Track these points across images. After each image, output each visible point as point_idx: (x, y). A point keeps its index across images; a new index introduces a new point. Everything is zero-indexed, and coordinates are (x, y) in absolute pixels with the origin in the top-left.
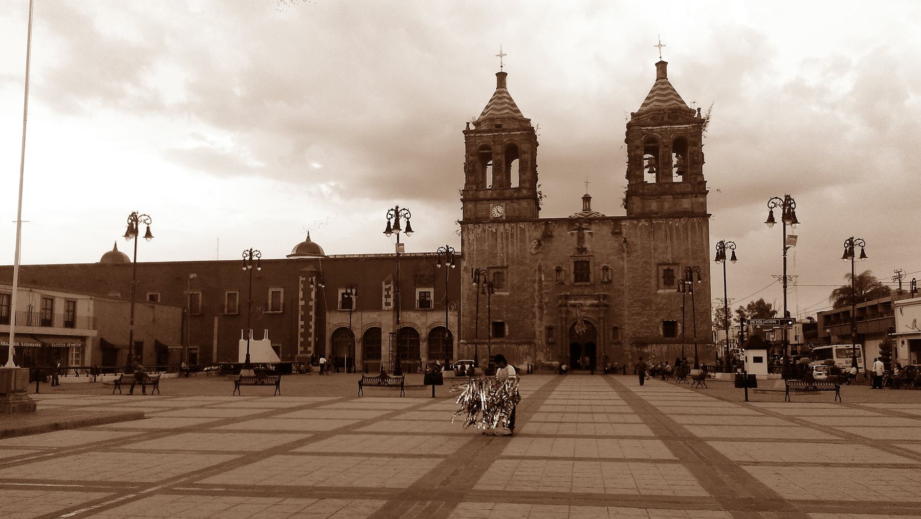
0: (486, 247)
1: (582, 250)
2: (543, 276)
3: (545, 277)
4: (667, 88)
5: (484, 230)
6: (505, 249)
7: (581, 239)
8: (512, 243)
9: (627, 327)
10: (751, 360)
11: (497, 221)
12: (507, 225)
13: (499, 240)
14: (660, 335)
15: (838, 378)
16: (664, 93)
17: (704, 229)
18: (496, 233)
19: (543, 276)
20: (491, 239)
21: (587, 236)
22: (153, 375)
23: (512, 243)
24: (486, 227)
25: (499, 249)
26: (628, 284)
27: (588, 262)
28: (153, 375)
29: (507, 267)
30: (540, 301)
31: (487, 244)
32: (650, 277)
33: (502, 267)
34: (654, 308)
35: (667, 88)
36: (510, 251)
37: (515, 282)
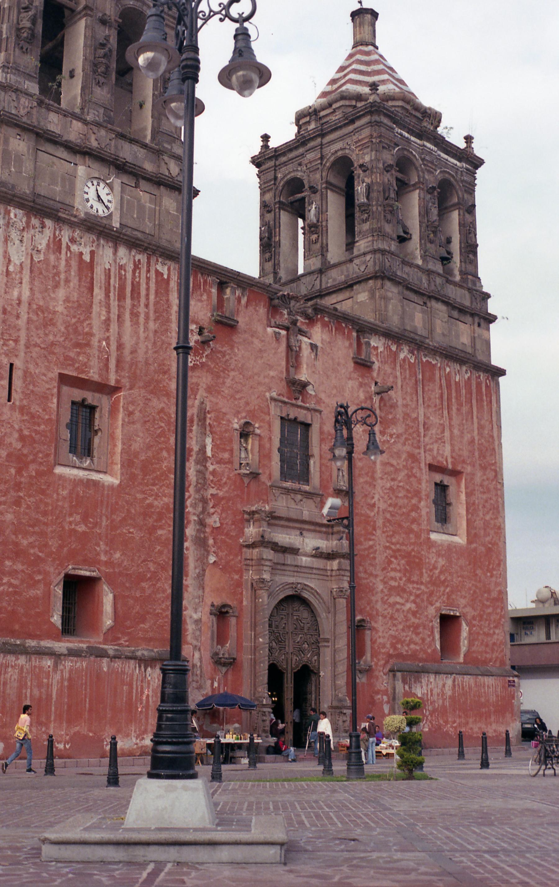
0: (59, 301)
1: (298, 388)
2: (209, 441)
3: (215, 447)
4: (376, 62)
5: (56, 245)
6: (114, 327)
7: (293, 356)
8: (135, 315)
9: (379, 624)
10: (345, 719)
11: (96, 227)
12: (122, 251)
13: (98, 293)
14: (435, 650)
15: (225, 753)
16: (369, 69)
17: (494, 398)
18: (91, 266)
19: (209, 441)
20: (74, 281)
21: (306, 352)
22: (390, 417)
23: (135, 315)
24: (65, 235)
25: (96, 323)
26: (382, 505)
27: (307, 426)
28: (390, 417)
29: (116, 389)
30: (202, 523)
31: (61, 293)
32: (417, 493)
33: (103, 388)
34: (426, 578)
35: (376, 62)
36: (128, 340)
37: (136, 446)
